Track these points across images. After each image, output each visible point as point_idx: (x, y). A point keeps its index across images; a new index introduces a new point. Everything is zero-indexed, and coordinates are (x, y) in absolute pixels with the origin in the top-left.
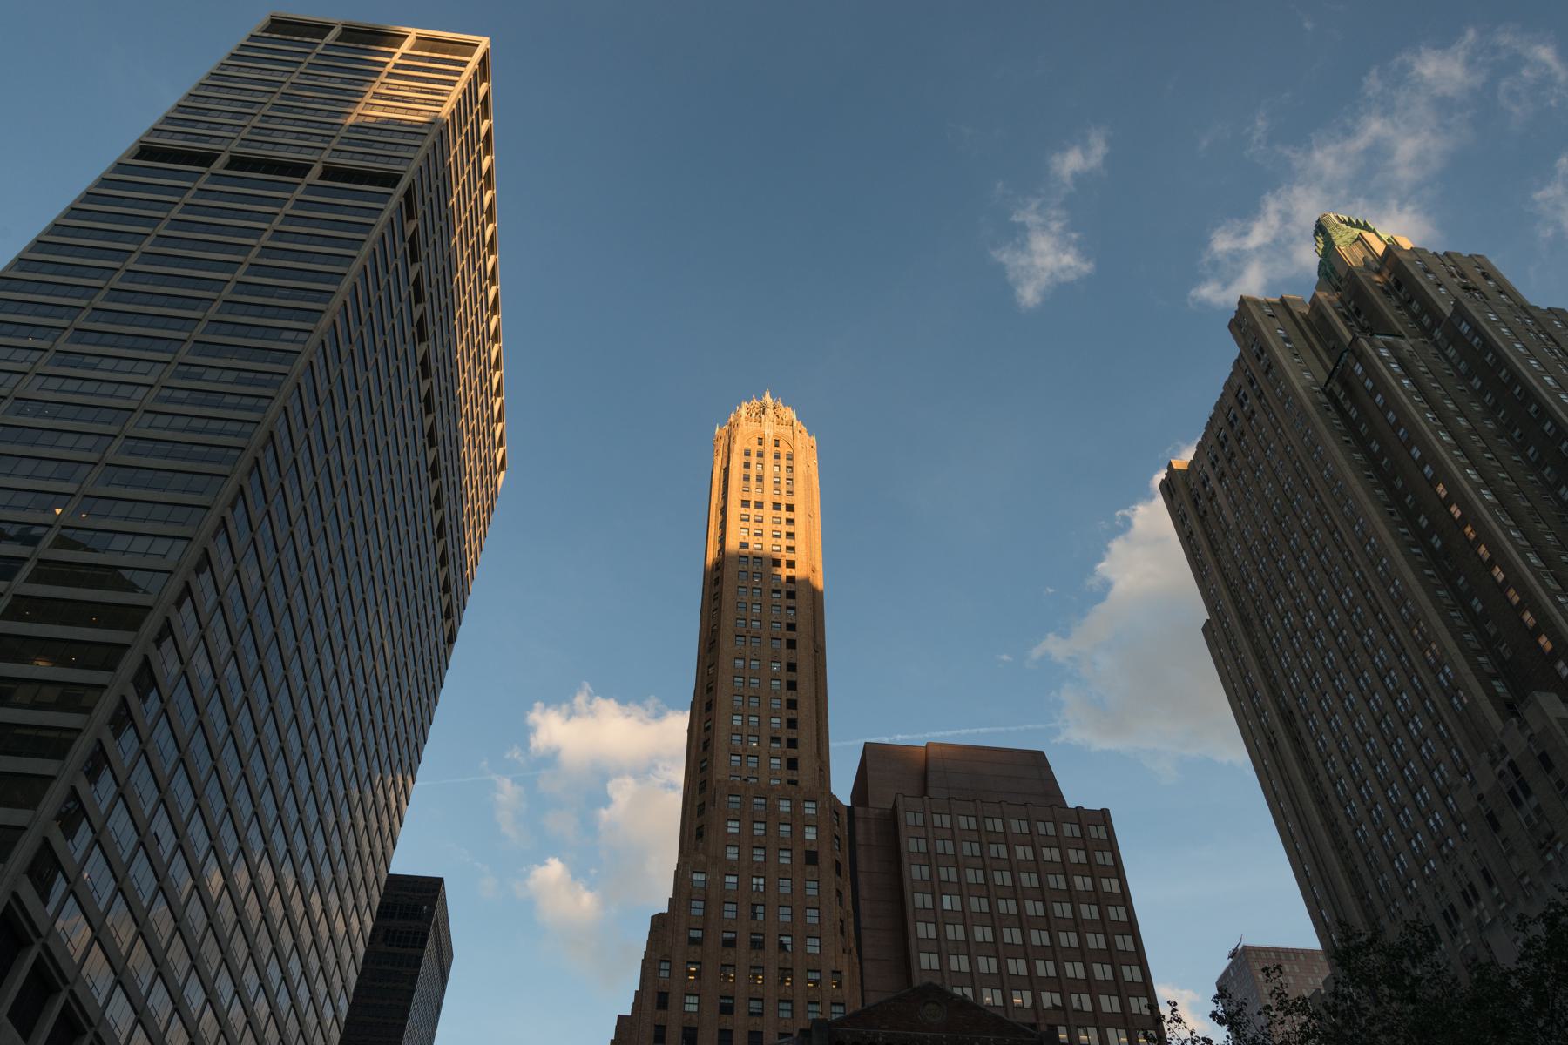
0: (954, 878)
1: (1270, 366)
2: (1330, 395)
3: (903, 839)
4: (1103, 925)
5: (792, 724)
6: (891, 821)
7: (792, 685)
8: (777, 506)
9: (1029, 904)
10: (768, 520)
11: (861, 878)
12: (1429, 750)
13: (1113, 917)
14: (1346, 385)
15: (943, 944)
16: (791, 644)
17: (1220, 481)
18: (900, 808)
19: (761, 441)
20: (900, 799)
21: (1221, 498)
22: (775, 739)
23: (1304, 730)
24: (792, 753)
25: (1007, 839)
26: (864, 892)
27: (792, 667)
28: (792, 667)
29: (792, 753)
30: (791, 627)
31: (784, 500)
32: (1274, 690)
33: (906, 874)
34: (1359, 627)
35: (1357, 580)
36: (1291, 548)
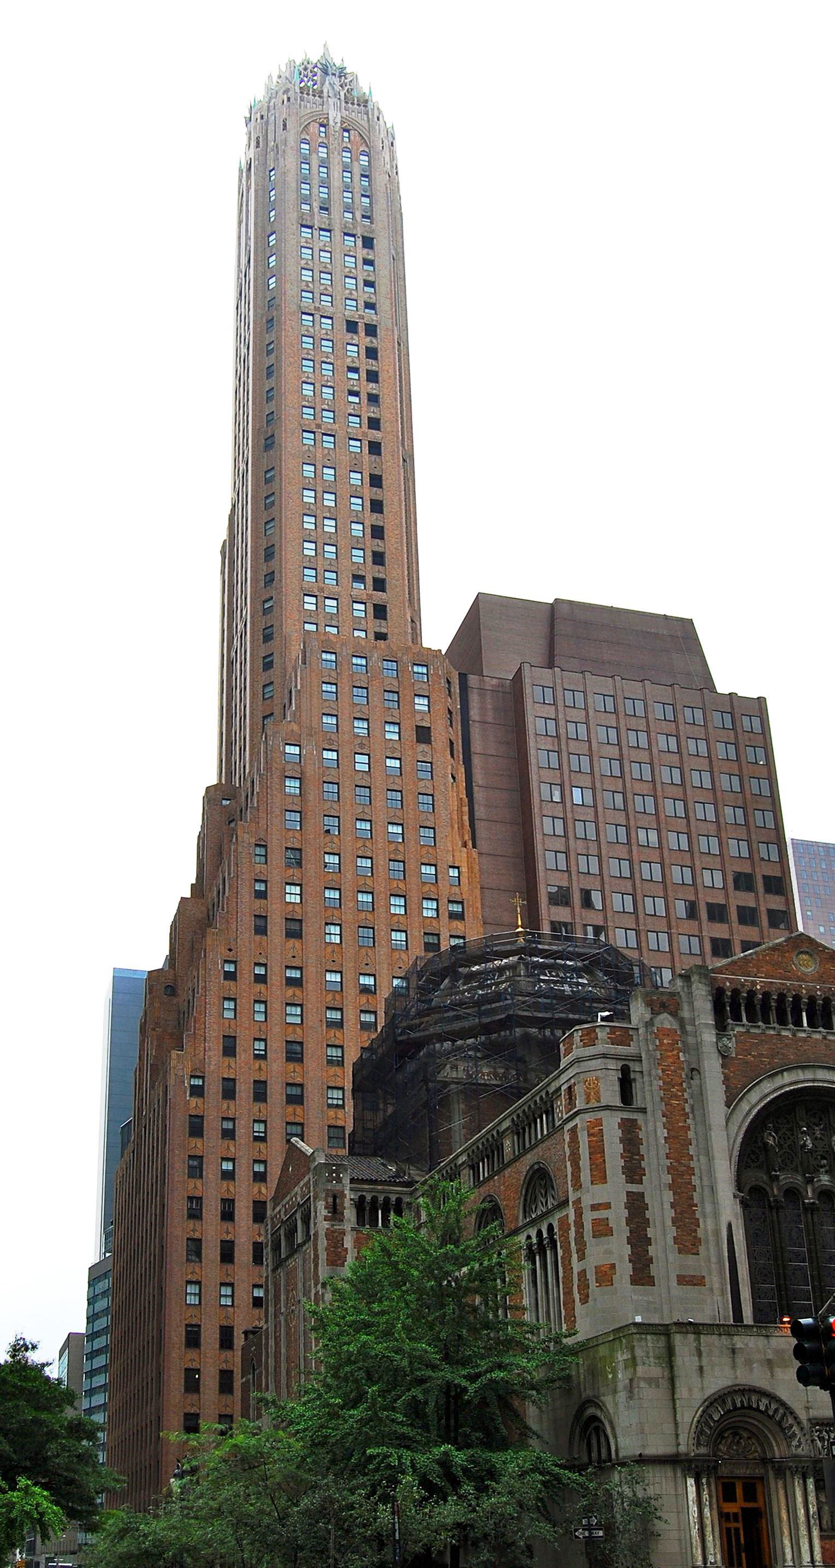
3: (530, 719)
5: (378, 558)
6: (513, 697)
7: (377, 506)
11: (476, 761)
18: (527, 681)
20: (527, 667)
22: (358, 578)
24: (379, 597)
27: (376, 481)
28: (376, 481)
29: (379, 597)
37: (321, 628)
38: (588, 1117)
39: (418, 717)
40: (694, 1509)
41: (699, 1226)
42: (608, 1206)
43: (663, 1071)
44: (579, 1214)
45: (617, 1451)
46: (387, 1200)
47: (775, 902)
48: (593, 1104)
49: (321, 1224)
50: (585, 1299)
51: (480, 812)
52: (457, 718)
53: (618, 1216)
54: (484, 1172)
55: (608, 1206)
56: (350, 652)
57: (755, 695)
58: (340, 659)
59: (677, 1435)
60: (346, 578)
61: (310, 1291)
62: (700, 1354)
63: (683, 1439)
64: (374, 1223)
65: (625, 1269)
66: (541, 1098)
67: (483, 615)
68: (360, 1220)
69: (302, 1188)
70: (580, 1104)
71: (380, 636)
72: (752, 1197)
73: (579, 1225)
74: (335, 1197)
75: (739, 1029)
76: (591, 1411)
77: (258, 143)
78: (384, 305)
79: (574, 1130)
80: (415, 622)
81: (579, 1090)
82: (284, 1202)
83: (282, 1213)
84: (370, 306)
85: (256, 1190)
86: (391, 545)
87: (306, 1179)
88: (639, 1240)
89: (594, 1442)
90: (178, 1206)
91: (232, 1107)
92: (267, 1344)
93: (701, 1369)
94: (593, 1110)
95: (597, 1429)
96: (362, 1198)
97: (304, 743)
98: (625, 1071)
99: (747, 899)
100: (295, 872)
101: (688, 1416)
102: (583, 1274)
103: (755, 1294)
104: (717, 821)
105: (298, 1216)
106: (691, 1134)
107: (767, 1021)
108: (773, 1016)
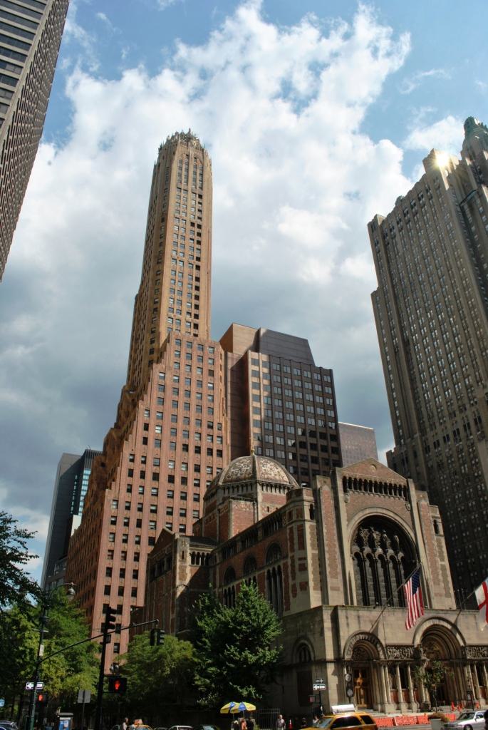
1: (439, 187)
2: (462, 209)
9: (297, 405)
12: (466, 370)
14: (471, 207)
15: (285, 422)
17: (400, 231)
21: (398, 239)
23: (412, 349)
29: (196, 321)
32: (402, 329)
34: (450, 313)
35: (454, 294)
36: (427, 272)
44: (293, 561)
45: (315, 658)
47: (334, 444)
50: (295, 596)
52: (223, 368)
57: (328, 369)
61: (170, 590)
68: (193, 562)
71: (196, 335)
73: (293, 566)
74: (183, 552)
76: (302, 641)
78: (204, 218)
84: (200, 218)
89: (303, 653)
90: (103, 552)
91: (129, 514)
92: (145, 614)
93: (348, 624)
95: (304, 649)
96: (194, 553)
99: (313, 441)
100: (160, 422)
102: (294, 586)
104: (315, 413)
108: (363, 488)
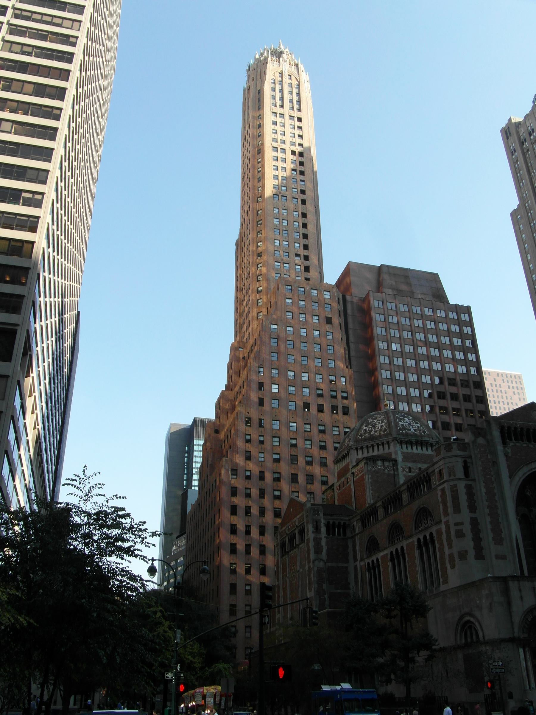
0: (397, 335)
4: (461, 335)
5: (306, 247)
8: (292, 117)
10: (287, 126)
11: (351, 332)
13: (463, 318)
16: (303, 202)
19: (281, 74)
22: (297, 255)
24: (307, 263)
25: (422, 316)
26: (351, 339)
28: (304, 215)
30: (303, 192)
31: (296, 114)
33: (375, 332)
37: (282, 276)
38: (452, 483)
39: (326, 313)
40: (523, 663)
41: (502, 532)
42: (462, 523)
43: (482, 462)
45: (484, 637)
46: (339, 523)
48: (452, 477)
49: (310, 534)
50: (453, 566)
51: (353, 353)
53: (467, 528)
54: (391, 509)
55: (462, 523)
56: (298, 285)
58: (293, 288)
59: (513, 629)
60: (292, 255)
62: (520, 590)
63: (516, 630)
64: (334, 534)
65: (472, 553)
66: (424, 475)
67: (350, 270)
69: (298, 519)
70: (446, 477)
72: (524, 520)
74: (317, 522)
75: (512, 444)
76: (468, 618)
77: (253, 80)
79: (443, 490)
80: (321, 273)
81: (445, 471)
82: (288, 525)
83: (286, 530)
85: (261, 520)
86: (311, 242)
87: (301, 514)
88: (477, 539)
89: (468, 633)
94: (453, 480)
95: (470, 627)
96: (328, 523)
97: (279, 323)
98: (465, 462)
101: (517, 620)
102: (451, 556)
103: (528, 564)
105: (297, 532)
106: (496, 491)
107: (523, 441)
